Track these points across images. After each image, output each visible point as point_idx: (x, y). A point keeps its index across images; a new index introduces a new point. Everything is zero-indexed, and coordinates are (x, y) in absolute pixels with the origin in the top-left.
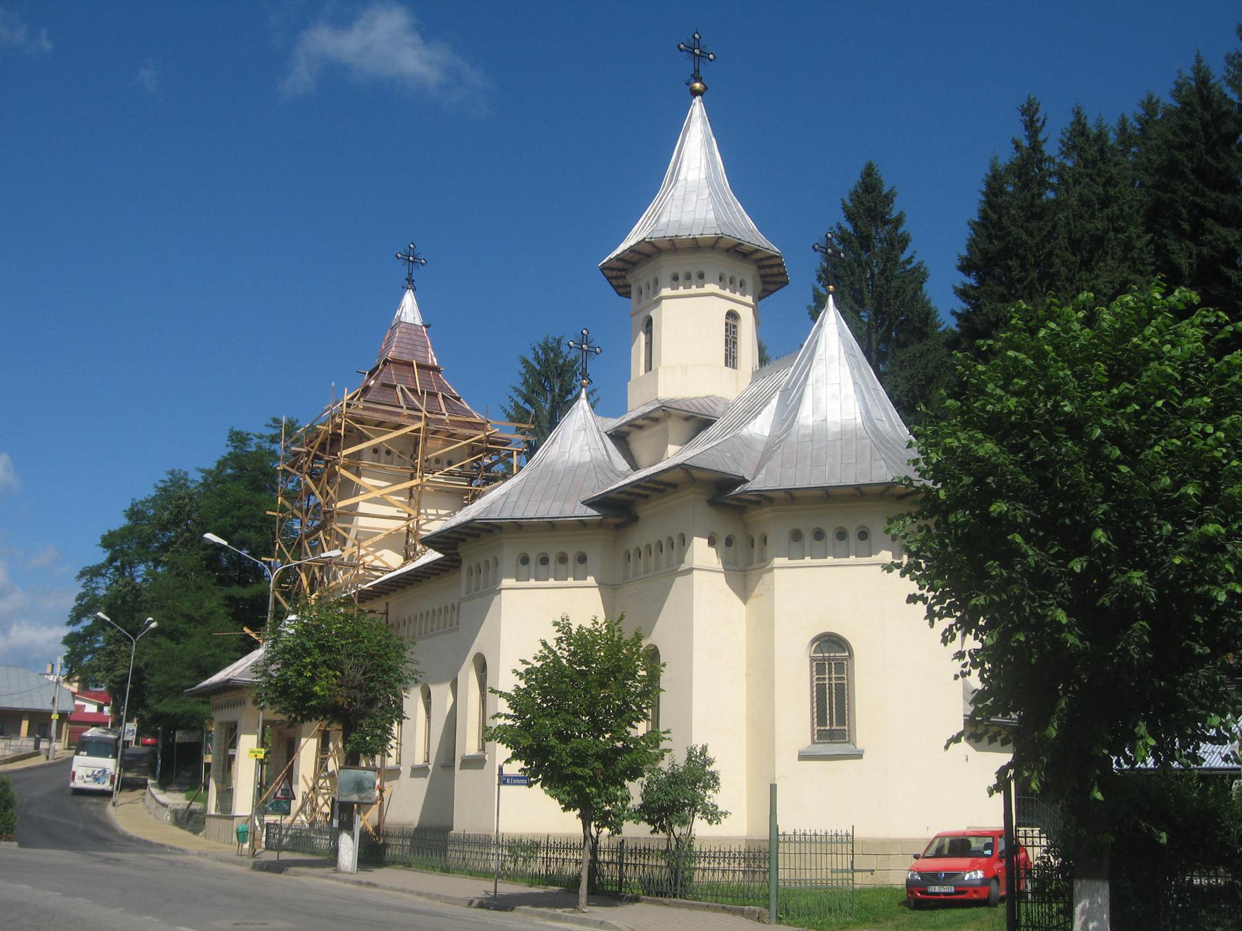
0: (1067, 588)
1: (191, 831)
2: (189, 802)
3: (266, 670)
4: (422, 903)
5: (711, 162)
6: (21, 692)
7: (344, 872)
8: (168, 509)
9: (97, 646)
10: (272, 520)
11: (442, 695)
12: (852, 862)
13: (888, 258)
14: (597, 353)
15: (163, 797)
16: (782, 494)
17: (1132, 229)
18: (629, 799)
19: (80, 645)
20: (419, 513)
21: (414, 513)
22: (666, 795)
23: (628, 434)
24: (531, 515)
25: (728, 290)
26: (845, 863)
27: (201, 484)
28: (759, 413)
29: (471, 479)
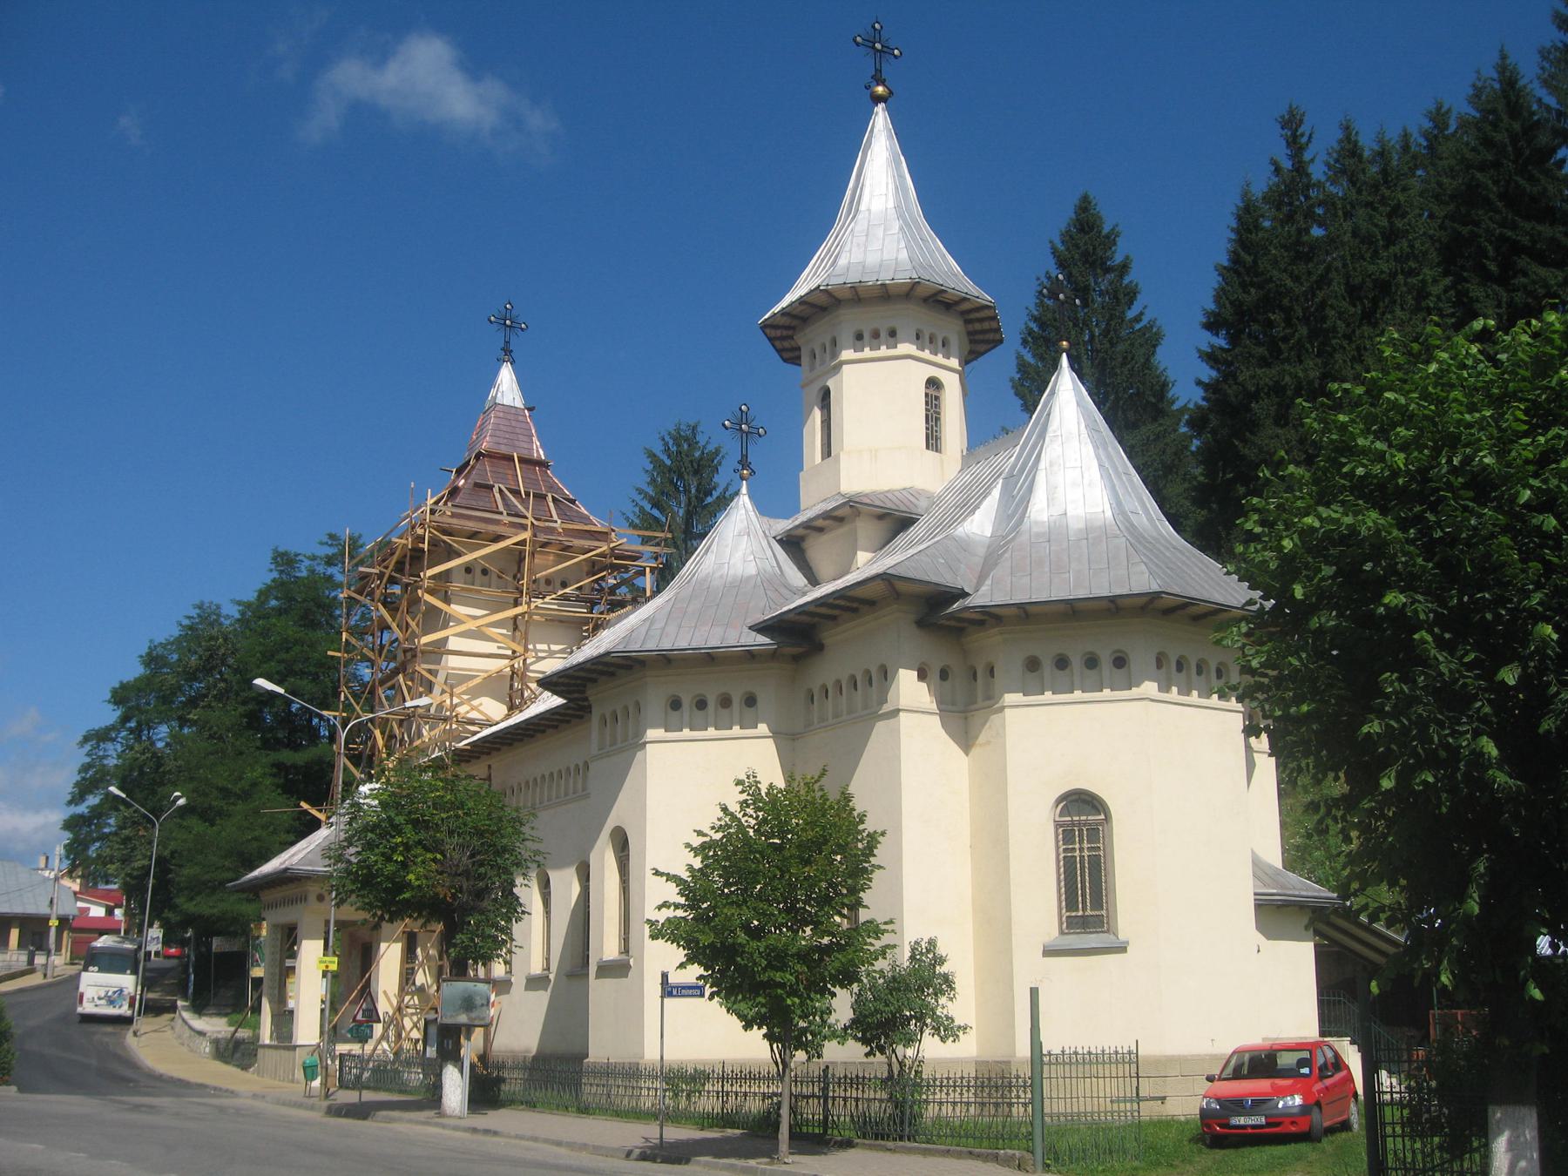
0: (1487, 710)
1: (238, 1066)
2: (233, 1029)
3: (341, 855)
4: (564, 1155)
5: (900, 188)
6: (8, 893)
7: (450, 1117)
8: (196, 653)
9: (106, 830)
10: (333, 664)
11: (566, 885)
12: (1137, 1088)
13: (1111, 315)
14: (760, 436)
15: (199, 1023)
16: (1014, 611)
17: (1426, 271)
18: (831, 1012)
19: (85, 830)
20: (526, 650)
21: (520, 649)
22: (887, 1005)
23: (802, 538)
24: (684, 645)
25: (927, 351)
26: (1128, 1089)
27: (238, 620)
28: (977, 507)
29: (592, 604)
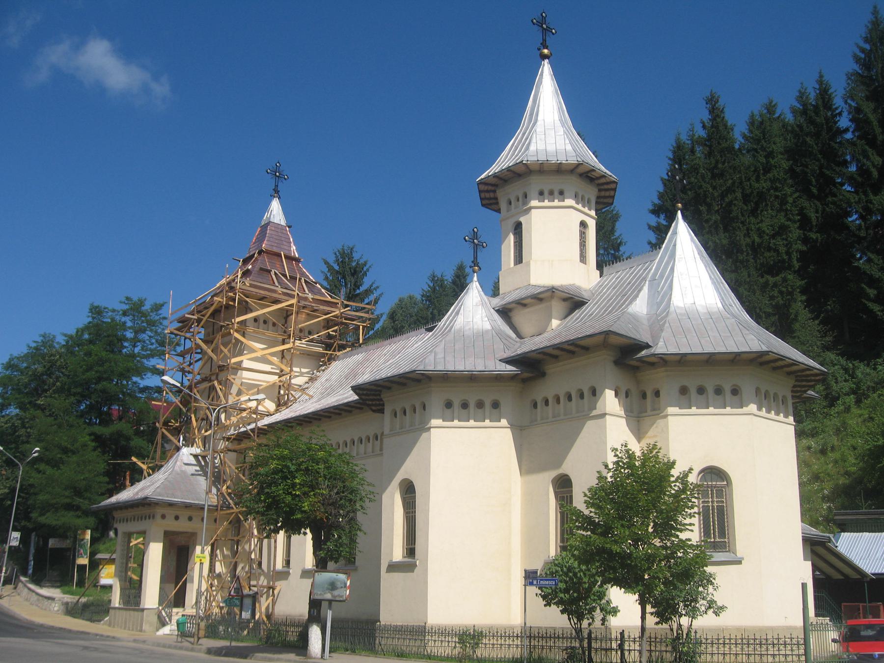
7: (315, 658)
14: (483, 247)
20: (291, 370)
21: (287, 369)
23: (510, 310)
25: (580, 205)
27: (64, 345)
